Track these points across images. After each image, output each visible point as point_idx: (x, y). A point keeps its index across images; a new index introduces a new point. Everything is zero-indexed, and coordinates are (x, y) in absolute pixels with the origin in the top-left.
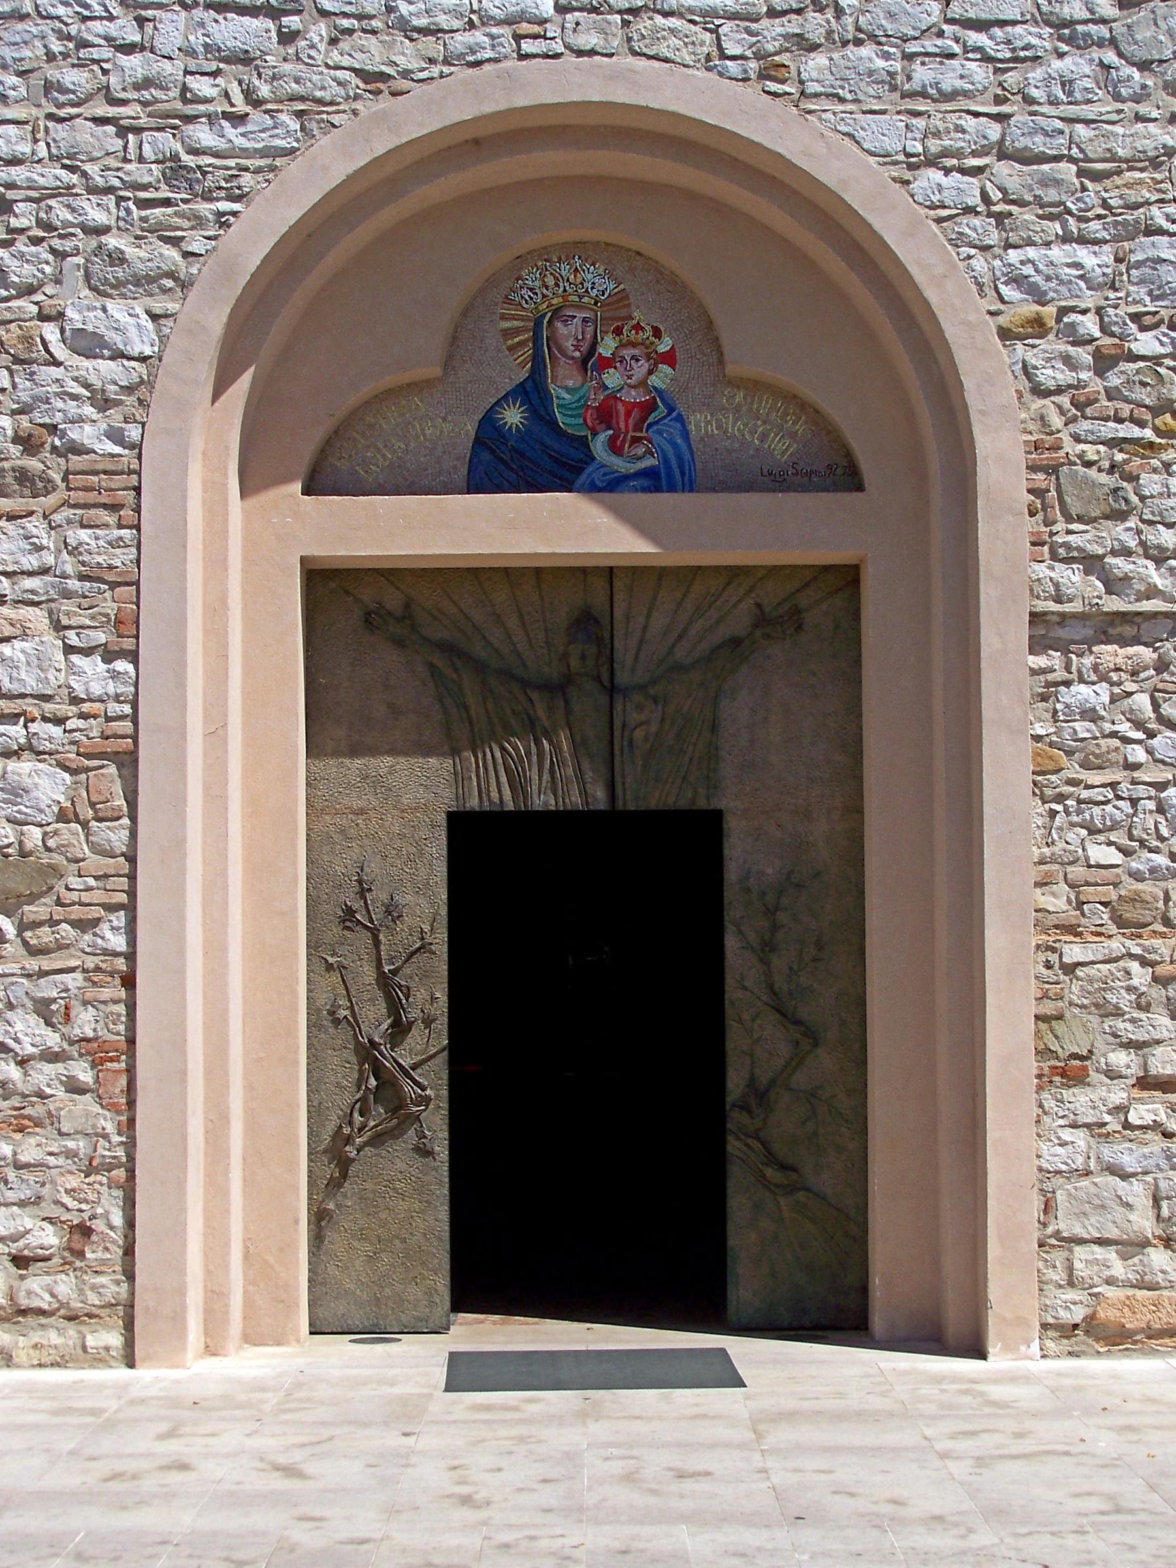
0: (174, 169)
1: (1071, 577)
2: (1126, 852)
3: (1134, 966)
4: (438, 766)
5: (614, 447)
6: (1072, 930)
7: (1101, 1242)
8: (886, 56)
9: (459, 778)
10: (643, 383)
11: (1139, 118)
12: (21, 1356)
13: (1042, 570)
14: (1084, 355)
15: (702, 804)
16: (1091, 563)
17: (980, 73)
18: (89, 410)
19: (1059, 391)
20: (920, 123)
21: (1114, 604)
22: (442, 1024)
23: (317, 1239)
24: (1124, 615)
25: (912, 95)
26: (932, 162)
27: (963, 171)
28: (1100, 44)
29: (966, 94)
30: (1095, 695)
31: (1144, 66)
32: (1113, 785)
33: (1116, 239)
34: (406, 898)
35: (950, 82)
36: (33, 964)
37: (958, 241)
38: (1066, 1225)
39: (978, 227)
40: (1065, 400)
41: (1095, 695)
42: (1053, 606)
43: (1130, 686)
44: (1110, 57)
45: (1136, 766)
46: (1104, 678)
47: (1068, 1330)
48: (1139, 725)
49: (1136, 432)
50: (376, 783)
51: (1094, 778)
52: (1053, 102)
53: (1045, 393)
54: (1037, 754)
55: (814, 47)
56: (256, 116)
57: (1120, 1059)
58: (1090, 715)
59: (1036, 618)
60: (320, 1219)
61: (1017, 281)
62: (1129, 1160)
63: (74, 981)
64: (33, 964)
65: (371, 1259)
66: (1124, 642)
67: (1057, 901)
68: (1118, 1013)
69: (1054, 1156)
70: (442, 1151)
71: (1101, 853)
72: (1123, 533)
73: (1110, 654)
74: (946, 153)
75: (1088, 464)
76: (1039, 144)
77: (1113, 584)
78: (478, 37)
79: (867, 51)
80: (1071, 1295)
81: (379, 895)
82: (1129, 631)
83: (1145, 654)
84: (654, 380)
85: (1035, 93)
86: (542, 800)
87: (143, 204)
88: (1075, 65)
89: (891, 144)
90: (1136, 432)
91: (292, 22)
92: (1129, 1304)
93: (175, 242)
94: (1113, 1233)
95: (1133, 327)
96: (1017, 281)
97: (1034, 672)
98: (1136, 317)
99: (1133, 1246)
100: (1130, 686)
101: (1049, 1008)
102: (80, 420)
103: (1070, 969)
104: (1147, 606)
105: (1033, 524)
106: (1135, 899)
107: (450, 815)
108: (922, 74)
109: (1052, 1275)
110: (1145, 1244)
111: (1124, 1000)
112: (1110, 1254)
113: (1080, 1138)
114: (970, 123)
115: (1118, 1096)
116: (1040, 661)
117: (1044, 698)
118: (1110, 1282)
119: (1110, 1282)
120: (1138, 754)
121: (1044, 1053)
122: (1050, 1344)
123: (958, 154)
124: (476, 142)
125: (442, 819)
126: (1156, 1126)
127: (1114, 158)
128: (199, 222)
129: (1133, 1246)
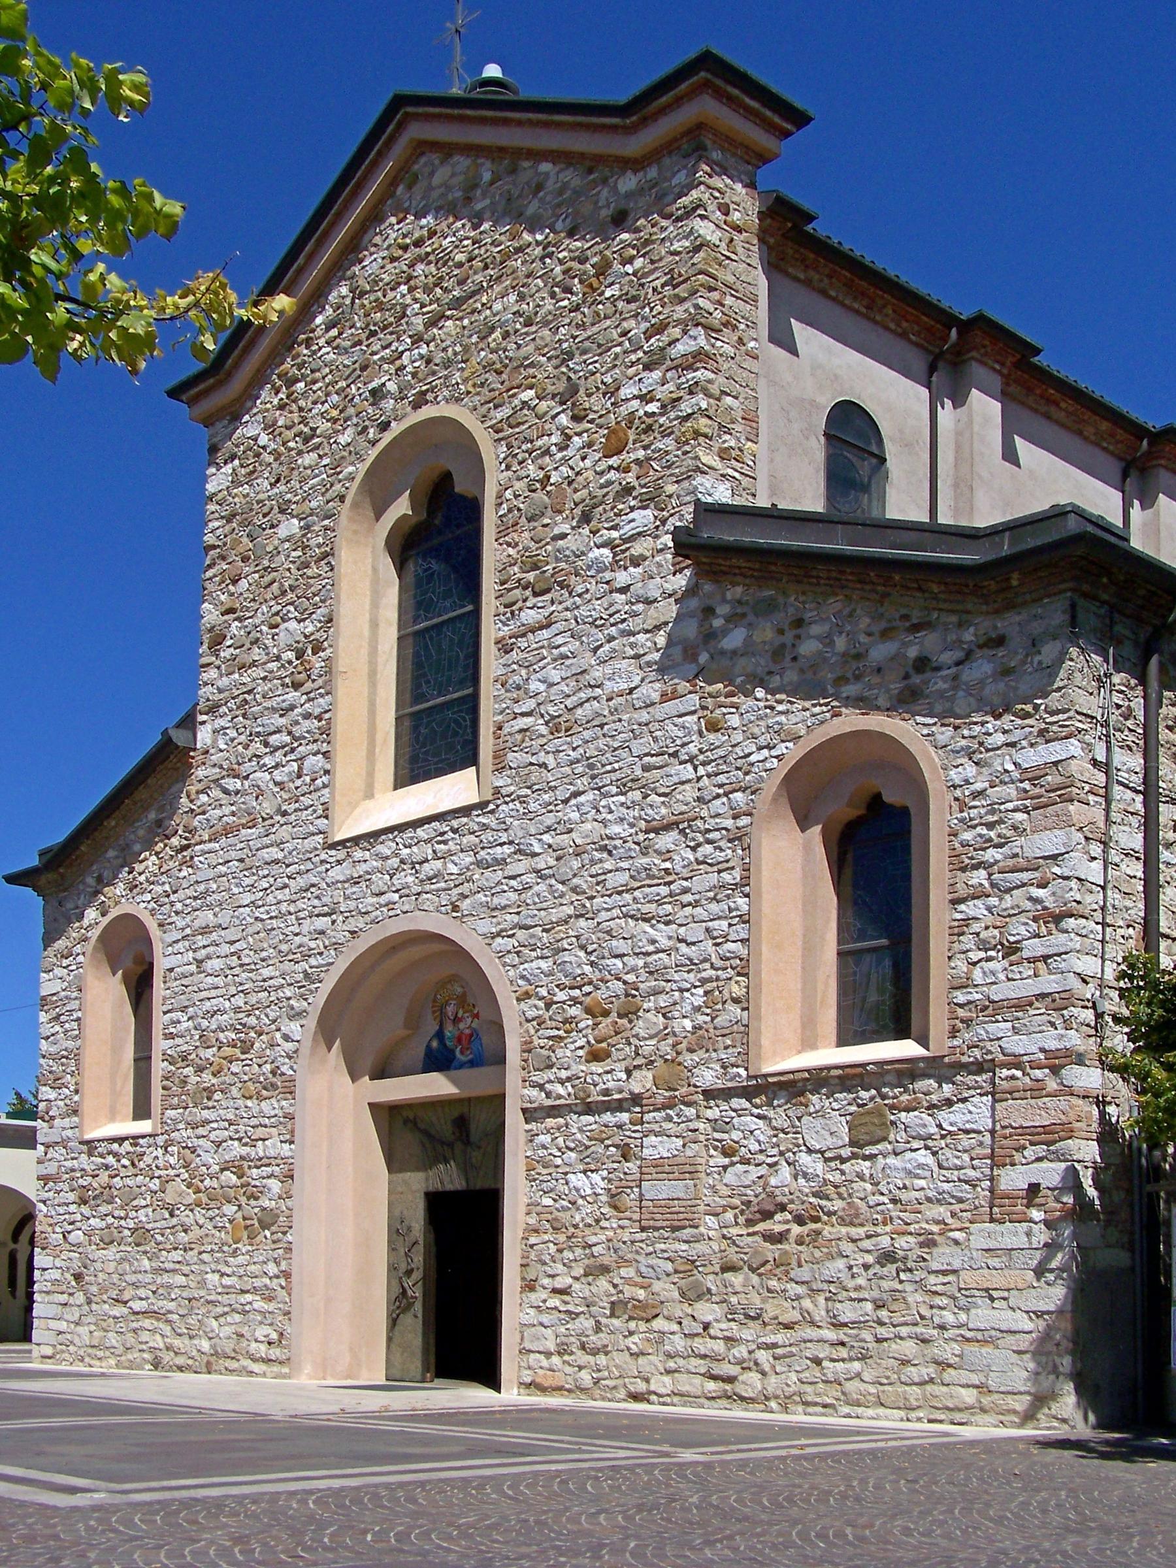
0: (306, 975)
1: (534, 1093)
2: (555, 1200)
3: (551, 1245)
4: (421, 1175)
5: (462, 1052)
6: (536, 1231)
7: (539, 1352)
8: (486, 896)
9: (427, 1179)
10: (470, 1027)
11: (562, 905)
12: (268, 1374)
13: (526, 1091)
14: (541, 1004)
15: (493, 1186)
16: (541, 1087)
17: (513, 896)
18: (287, 1060)
19: (533, 1019)
20: (494, 920)
21: (549, 1102)
22: (421, 1270)
23: (388, 1347)
24: (553, 1107)
25: (493, 910)
26: (498, 934)
27: (509, 936)
28: (550, 877)
29: (509, 906)
30: (545, 1139)
31: (563, 883)
32: (550, 1174)
33: (553, 955)
34: (413, 1224)
35: (504, 902)
36: (274, 1246)
37: (504, 965)
38: (527, 1345)
39: (511, 959)
40: (535, 1023)
41: (545, 1139)
42: (529, 1105)
43: (557, 1135)
44: (553, 882)
45: (557, 1167)
46: (548, 1132)
47: (528, 1386)
48: (559, 1150)
49: (556, 1032)
50: (405, 1182)
51: (544, 1171)
52: (535, 904)
53: (528, 1021)
54: (527, 1164)
55: (467, 897)
56: (326, 953)
57: (546, 1281)
58: (544, 1147)
59: (524, 1111)
60: (390, 1340)
61: (523, 977)
62: (546, 1321)
63: (281, 1251)
64: (274, 1246)
65: (402, 1354)
66: (555, 1117)
67: (532, 1220)
68: (545, 1263)
69: (525, 1319)
70: (420, 1315)
71: (547, 1201)
72: (549, 1074)
73: (550, 1122)
74: (502, 931)
75: (542, 1048)
76: (529, 922)
77: (548, 1095)
78: (378, 912)
79: (480, 895)
80: (528, 1372)
81: (406, 1223)
82: (556, 1112)
83: (561, 1121)
84: (474, 1025)
85: (528, 901)
86: (449, 1187)
87: (300, 988)
88: (542, 888)
89: (485, 930)
90: (556, 1032)
91: (334, 917)
92: (545, 1376)
93: (306, 999)
94: (541, 1349)
95: (557, 990)
96: (523, 977)
97: (527, 1131)
98: (557, 986)
99: (548, 1354)
100: (557, 1135)
101: (524, 1261)
102: (284, 1064)
103: (532, 1246)
104: (558, 1102)
105: (524, 1074)
106: (556, 1219)
107: (428, 1195)
108: (496, 901)
109: (522, 1364)
110: (552, 1354)
111: (547, 1258)
112: (542, 1357)
113: (532, 1312)
114: (508, 917)
115: (544, 1296)
116: (528, 1127)
117: (531, 1141)
118: (541, 1368)
119: (541, 1368)
120: (558, 1161)
121: (523, 1279)
122: (522, 1391)
123: (506, 930)
124: (394, 948)
125: (423, 1195)
126: (556, 1308)
127: (552, 923)
128: (311, 992)
129: (548, 1354)
